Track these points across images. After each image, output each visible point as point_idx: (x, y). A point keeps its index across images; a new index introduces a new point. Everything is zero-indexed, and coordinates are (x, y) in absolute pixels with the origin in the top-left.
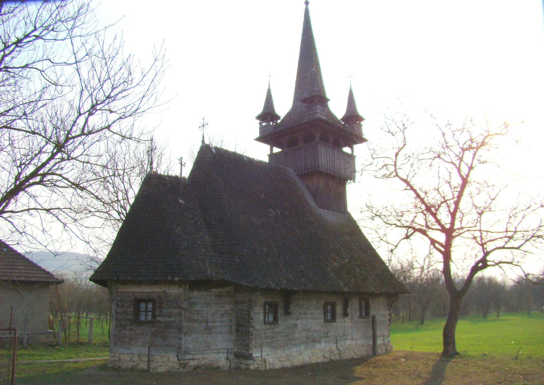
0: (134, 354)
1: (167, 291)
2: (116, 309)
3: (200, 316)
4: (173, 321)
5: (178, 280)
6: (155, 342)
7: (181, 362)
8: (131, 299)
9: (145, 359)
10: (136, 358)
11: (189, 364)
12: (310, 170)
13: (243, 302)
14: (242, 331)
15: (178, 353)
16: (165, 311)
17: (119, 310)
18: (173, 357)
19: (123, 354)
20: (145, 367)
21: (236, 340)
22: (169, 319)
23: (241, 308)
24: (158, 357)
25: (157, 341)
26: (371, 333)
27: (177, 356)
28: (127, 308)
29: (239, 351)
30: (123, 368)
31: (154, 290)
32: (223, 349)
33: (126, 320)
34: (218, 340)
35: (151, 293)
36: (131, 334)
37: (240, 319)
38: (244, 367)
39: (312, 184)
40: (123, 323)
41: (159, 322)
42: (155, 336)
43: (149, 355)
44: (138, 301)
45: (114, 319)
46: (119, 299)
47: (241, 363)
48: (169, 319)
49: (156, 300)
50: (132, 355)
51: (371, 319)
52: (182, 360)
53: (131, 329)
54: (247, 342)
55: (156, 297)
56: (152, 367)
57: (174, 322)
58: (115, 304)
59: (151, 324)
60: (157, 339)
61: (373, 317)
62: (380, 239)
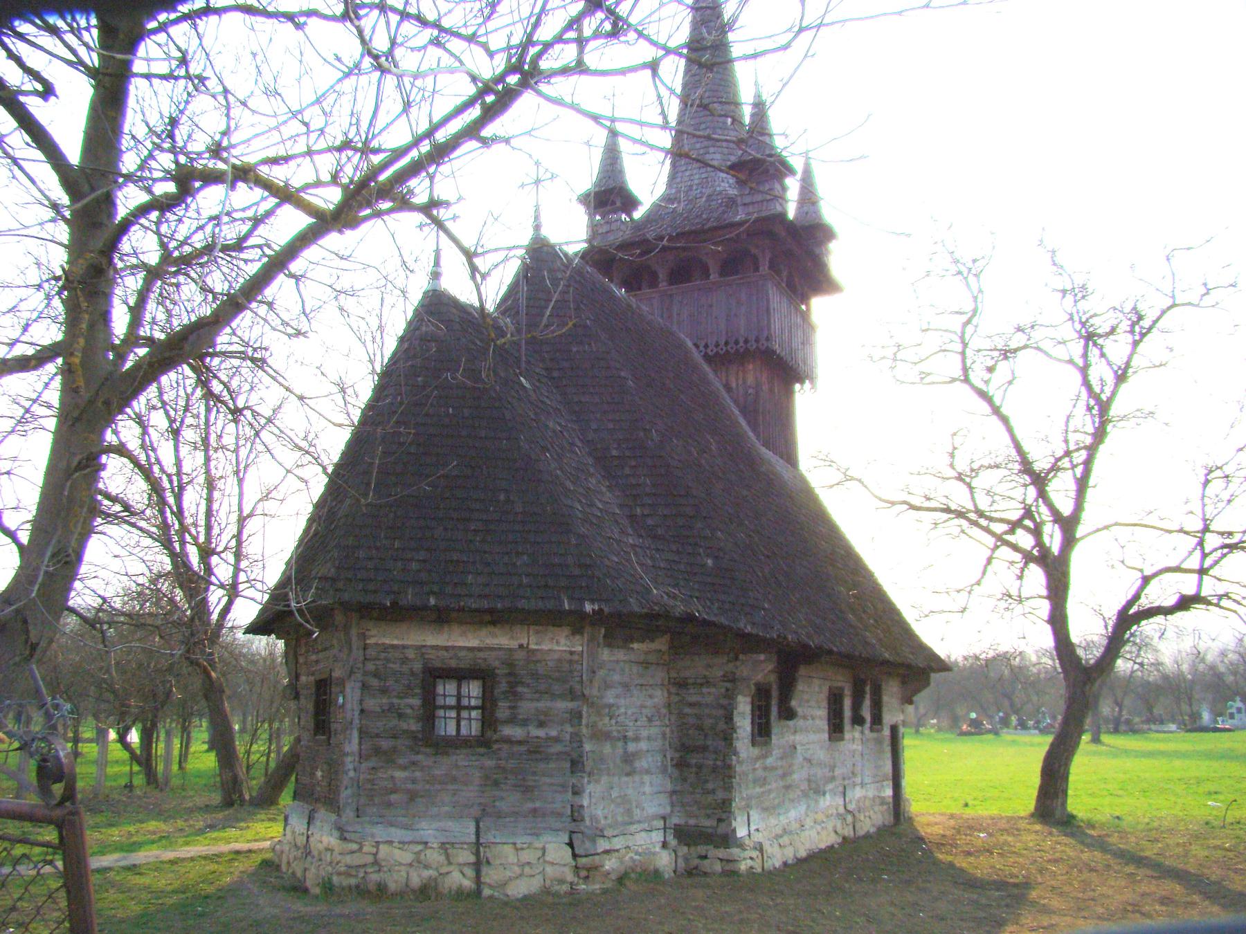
0: (426, 843)
1: (533, 647)
2: (361, 701)
3: (613, 721)
5: (593, 610)
6: (497, 804)
7: (583, 861)
8: (411, 669)
9: (467, 856)
10: (434, 856)
11: (602, 866)
12: (741, 344)
13: (707, 682)
14: (700, 767)
15: (574, 836)
16: (527, 707)
17: (372, 704)
18: (558, 851)
19: (390, 842)
20: (468, 883)
21: (673, 792)
22: (541, 733)
23: (693, 699)
24: (508, 849)
25: (502, 798)
26: (888, 767)
27: (571, 844)
29: (692, 822)
30: (392, 886)
31: (491, 641)
32: (655, 817)
33: (395, 737)
34: (644, 793)
35: (480, 649)
36: (414, 781)
37: (690, 732)
38: (718, 867)
39: (740, 382)
40: (385, 744)
41: (508, 741)
42: (496, 784)
43: (478, 844)
44: (434, 674)
45: (356, 734)
46: (370, 666)
47: (705, 857)
48: (541, 733)
49: (497, 671)
50: (420, 847)
51: (886, 732)
52: (586, 856)
53: (414, 763)
54: (720, 795)
55: (497, 663)
56: (488, 880)
57: (557, 740)
58: (359, 685)
59: (481, 746)
60: (497, 793)
61: (894, 729)
62: (959, 529)
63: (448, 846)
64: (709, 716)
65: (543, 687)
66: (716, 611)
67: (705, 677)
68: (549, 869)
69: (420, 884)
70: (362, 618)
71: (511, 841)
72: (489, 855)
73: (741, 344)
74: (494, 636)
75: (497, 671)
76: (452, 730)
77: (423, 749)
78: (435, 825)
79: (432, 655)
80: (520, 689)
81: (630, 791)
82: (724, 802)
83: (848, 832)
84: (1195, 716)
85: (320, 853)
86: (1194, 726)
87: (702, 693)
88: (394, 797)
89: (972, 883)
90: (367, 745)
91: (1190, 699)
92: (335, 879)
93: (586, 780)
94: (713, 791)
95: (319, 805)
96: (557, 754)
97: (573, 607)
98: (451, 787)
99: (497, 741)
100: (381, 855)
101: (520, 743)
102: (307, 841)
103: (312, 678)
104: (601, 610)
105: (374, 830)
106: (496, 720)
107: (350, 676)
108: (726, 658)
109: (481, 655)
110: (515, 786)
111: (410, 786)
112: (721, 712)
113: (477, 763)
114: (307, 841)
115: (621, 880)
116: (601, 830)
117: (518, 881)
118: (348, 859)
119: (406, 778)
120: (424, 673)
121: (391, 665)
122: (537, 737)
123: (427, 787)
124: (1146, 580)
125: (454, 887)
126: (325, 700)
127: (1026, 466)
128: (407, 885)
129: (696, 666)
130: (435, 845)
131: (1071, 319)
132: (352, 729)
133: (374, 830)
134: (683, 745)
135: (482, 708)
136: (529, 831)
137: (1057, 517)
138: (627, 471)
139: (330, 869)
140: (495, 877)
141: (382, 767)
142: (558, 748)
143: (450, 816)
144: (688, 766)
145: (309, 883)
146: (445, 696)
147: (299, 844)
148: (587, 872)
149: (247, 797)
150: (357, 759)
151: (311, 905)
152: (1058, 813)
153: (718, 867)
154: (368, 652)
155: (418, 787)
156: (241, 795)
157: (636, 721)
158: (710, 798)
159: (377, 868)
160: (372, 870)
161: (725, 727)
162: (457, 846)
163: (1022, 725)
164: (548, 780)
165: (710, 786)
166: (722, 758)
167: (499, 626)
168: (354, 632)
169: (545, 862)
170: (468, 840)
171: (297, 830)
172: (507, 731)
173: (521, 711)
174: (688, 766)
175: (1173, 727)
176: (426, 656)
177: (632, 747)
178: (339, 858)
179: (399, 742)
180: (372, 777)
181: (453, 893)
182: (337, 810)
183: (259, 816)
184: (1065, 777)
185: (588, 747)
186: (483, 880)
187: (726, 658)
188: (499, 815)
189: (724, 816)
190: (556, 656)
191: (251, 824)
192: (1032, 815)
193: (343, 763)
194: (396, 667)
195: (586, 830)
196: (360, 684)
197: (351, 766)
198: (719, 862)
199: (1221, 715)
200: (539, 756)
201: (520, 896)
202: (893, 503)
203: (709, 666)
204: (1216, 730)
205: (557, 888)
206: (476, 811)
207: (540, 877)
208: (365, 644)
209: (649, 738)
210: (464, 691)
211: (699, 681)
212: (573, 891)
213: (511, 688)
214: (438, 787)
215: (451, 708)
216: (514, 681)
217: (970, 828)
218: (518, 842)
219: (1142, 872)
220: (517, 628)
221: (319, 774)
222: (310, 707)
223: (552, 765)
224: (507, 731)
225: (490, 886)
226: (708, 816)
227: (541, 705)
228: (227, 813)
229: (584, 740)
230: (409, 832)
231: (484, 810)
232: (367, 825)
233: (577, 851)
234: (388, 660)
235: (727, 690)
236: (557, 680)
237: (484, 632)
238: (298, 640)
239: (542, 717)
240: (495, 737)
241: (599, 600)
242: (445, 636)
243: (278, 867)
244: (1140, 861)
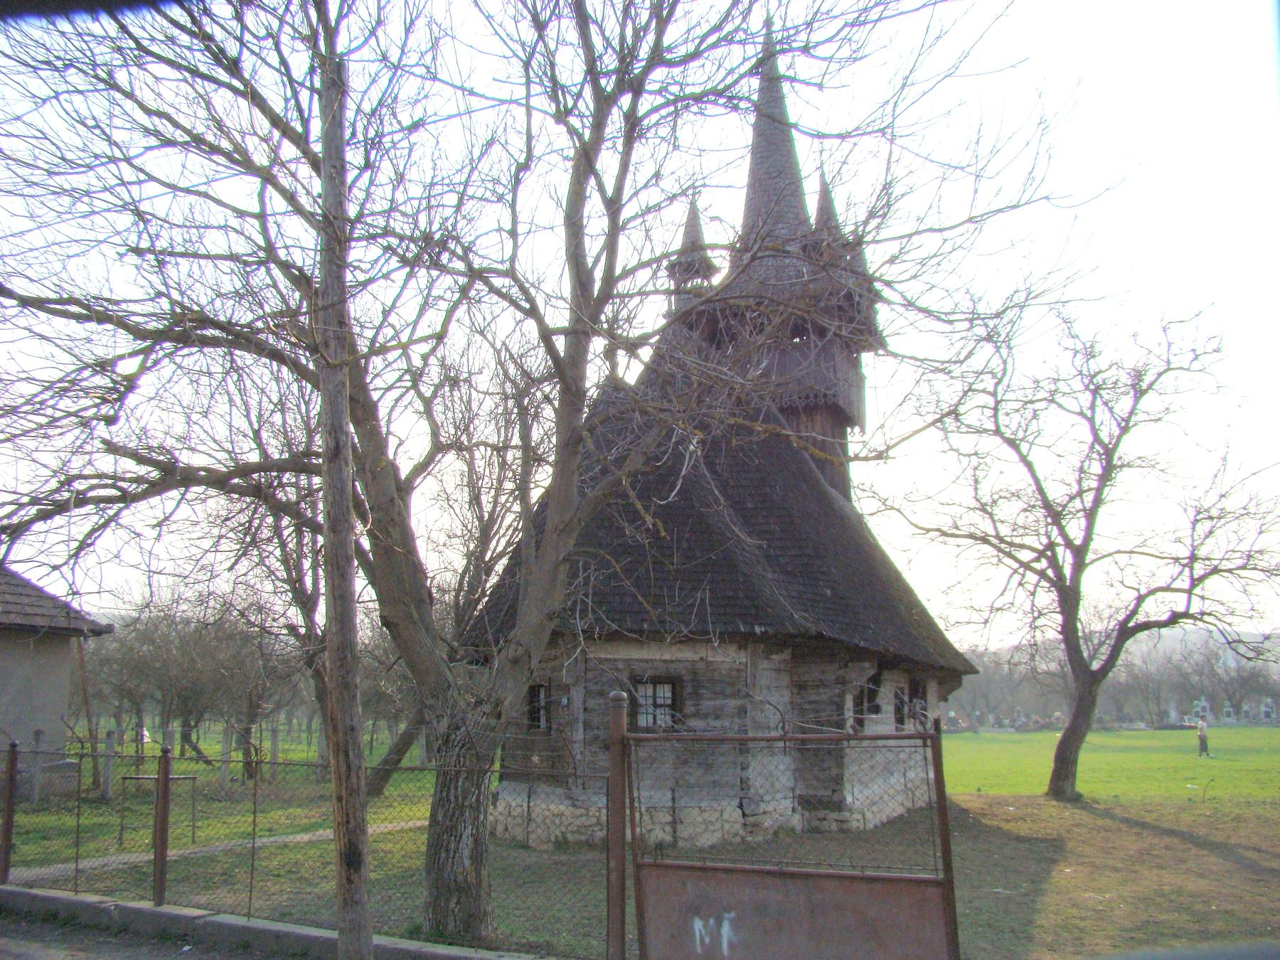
1: (710, 659)
2: (584, 702)
7: (751, 819)
12: (812, 398)
13: (822, 684)
16: (707, 705)
17: (591, 703)
20: (668, 838)
22: (717, 724)
24: (696, 812)
31: (680, 655)
35: (672, 662)
43: (674, 809)
45: (581, 726)
47: (825, 819)
54: (834, 771)
55: (684, 672)
65: (718, 689)
68: (727, 826)
73: (812, 398)
83: (909, 804)
84: (1163, 714)
86: (1161, 723)
89: (1020, 839)
91: (1158, 698)
92: (570, 837)
94: (829, 768)
109: (674, 666)
115: (776, 833)
124: (1140, 599)
127: (1047, 505)
129: (813, 672)
131: (1080, 373)
137: (1068, 544)
138: (761, 520)
148: (753, 828)
152: (1068, 793)
163: (999, 724)
165: (826, 765)
175: (1142, 725)
184: (1074, 762)
188: (689, 786)
192: (1047, 794)
199: (1186, 713)
202: (928, 531)
203: (823, 672)
204: (1183, 728)
206: (671, 783)
216: (697, 683)
217: (999, 803)
219: (1145, 833)
225: (683, 839)
227: (717, 702)
236: (729, 684)
244: (1143, 825)
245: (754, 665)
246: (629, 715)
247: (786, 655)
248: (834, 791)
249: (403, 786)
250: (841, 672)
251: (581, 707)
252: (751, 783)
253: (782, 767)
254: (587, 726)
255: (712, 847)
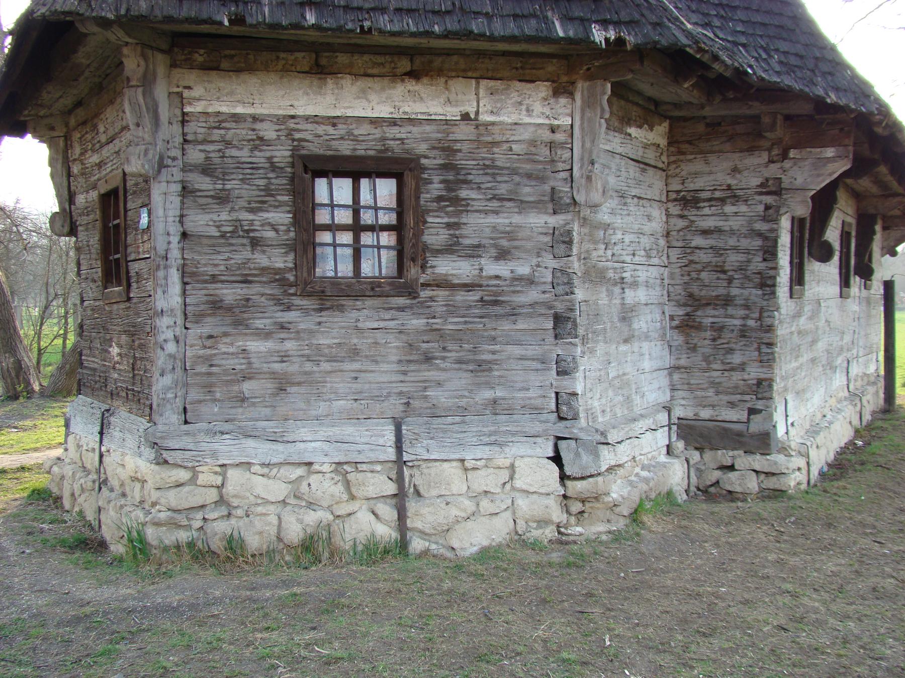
0: (310, 464)
1: (485, 118)
4: (520, 279)
8: (270, 159)
11: (607, 494)
13: (732, 196)
14: (719, 329)
15: (562, 445)
20: (385, 532)
22: (502, 269)
23: (710, 223)
24: (451, 470)
25: (439, 384)
27: (557, 459)
28: (252, 211)
29: (705, 414)
30: (253, 542)
35: (393, 122)
38: (752, 484)
40: (230, 294)
42: (428, 359)
43: (400, 462)
45: (175, 277)
46: (195, 155)
47: (731, 468)
48: (502, 269)
50: (300, 471)
51: (877, 289)
52: (583, 478)
53: (282, 327)
54: (754, 372)
55: (422, 148)
56: (419, 525)
57: (530, 281)
58: (178, 187)
60: (433, 375)
61: (889, 286)
63: (347, 468)
64: (735, 249)
66: (778, 68)
67: (729, 187)
68: (522, 503)
69: (302, 535)
70: (174, 65)
71: (457, 456)
72: (418, 480)
74: (417, 97)
75: (424, 161)
76: (346, 269)
77: (297, 301)
78: (325, 432)
79: (307, 132)
80: (464, 193)
81: (629, 368)
82: (759, 382)
85: (122, 485)
87: (725, 215)
88: (247, 387)
90: (197, 296)
92: (151, 533)
93: (579, 350)
94: (742, 367)
95: (116, 403)
96: (531, 305)
97: (571, 34)
98: (348, 366)
99: (425, 285)
100: (230, 489)
101: (468, 287)
102: (101, 462)
103: (94, 195)
104: (620, 41)
105: (216, 446)
106: (426, 248)
107: (159, 171)
108: (765, 156)
110: (459, 361)
111: (277, 367)
112: (758, 242)
113: (392, 324)
114: (101, 462)
115: (635, 516)
116: (603, 434)
117: (470, 524)
118: (173, 498)
119: (270, 353)
120: (293, 165)
121: (234, 152)
122: (497, 277)
123: (308, 367)
125: (362, 538)
126: (117, 226)
128: (279, 539)
130: (326, 468)
132: (166, 267)
133: (216, 446)
134: (691, 295)
135: (398, 228)
136: (486, 439)
139: (140, 514)
140: (430, 518)
141: (226, 334)
142: (533, 295)
143: (352, 418)
144: (699, 327)
145: (107, 533)
146: (332, 206)
147: (89, 466)
149: (37, 387)
150: (180, 321)
151: (108, 582)
153: (752, 484)
154: (191, 128)
155: (292, 368)
156: (28, 384)
157: (634, 255)
158: (736, 376)
159: (224, 511)
160: (215, 515)
161: (762, 266)
162: (364, 467)
164: (517, 351)
165: (736, 359)
166: (756, 315)
167: (425, 80)
168: (161, 92)
169: (513, 488)
170: (382, 457)
171: (83, 442)
172: (444, 266)
173: (464, 231)
174: (699, 327)
176: (297, 136)
177: (630, 296)
178: (155, 495)
179: (256, 289)
180: (209, 352)
181: (360, 548)
182: (149, 412)
183: (51, 411)
185: (580, 294)
186: (409, 523)
187: (765, 156)
189: (759, 405)
190: (526, 135)
191: (38, 422)
193: (154, 328)
194: (244, 154)
195: (582, 435)
196: (179, 187)
197: (169, 335)
198: (754, 474)
200: (498, 310)
201: (474, 549)
203: (735, 170)
205: (536, 533)
206: (394, 406)
207: (508, 515)
208: (184, 114)
209: (647, 285)
210: (365, 197)
211: (718, 194)
212: (562, 541)
213: (449, 190)
214: (326, 366)
215: (344, 228)
218: (468, 456)
220: (457, 85)
221: (115, 350)
222: (94, 240)
223: (521, 325)
224: (444, 266)
225: (423, 534)
226: (732, 405)
228: (7, 409)
229: (576, 282)
230: (280, 447)
231: (408, 404)
232: (201, 437)
233: (568, 471)
234: (228, 144)
235: (767, 208)
237: (400, 90)
238: (67, 138)
239: (504, 243)
240: (423, 279)
241: (617, 24)
242: (330, 99)
243: (58, 499)
245: (590, 133)
246: (857, 254)
247: (658, 135)
248: (752, 411)
249: (161, 338)
250: (773, 170)
251: (175, 230)
252: (581, 405)
253: (647, 365)
254: (188, 276)
255: (486, 554)
